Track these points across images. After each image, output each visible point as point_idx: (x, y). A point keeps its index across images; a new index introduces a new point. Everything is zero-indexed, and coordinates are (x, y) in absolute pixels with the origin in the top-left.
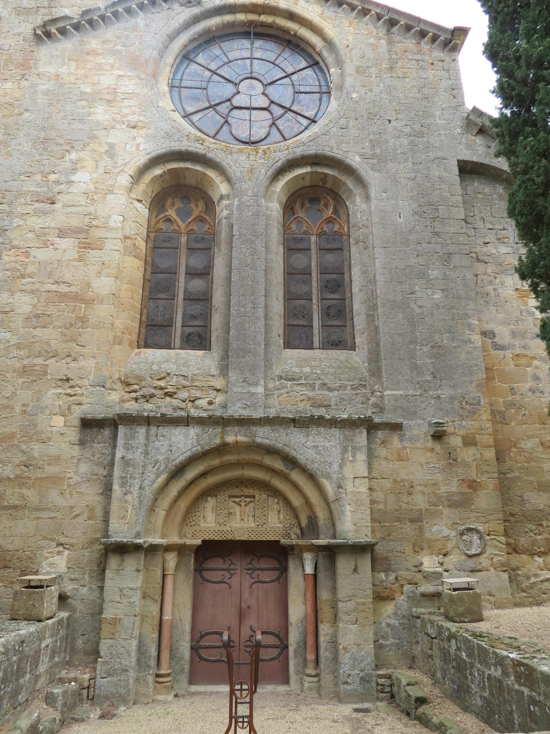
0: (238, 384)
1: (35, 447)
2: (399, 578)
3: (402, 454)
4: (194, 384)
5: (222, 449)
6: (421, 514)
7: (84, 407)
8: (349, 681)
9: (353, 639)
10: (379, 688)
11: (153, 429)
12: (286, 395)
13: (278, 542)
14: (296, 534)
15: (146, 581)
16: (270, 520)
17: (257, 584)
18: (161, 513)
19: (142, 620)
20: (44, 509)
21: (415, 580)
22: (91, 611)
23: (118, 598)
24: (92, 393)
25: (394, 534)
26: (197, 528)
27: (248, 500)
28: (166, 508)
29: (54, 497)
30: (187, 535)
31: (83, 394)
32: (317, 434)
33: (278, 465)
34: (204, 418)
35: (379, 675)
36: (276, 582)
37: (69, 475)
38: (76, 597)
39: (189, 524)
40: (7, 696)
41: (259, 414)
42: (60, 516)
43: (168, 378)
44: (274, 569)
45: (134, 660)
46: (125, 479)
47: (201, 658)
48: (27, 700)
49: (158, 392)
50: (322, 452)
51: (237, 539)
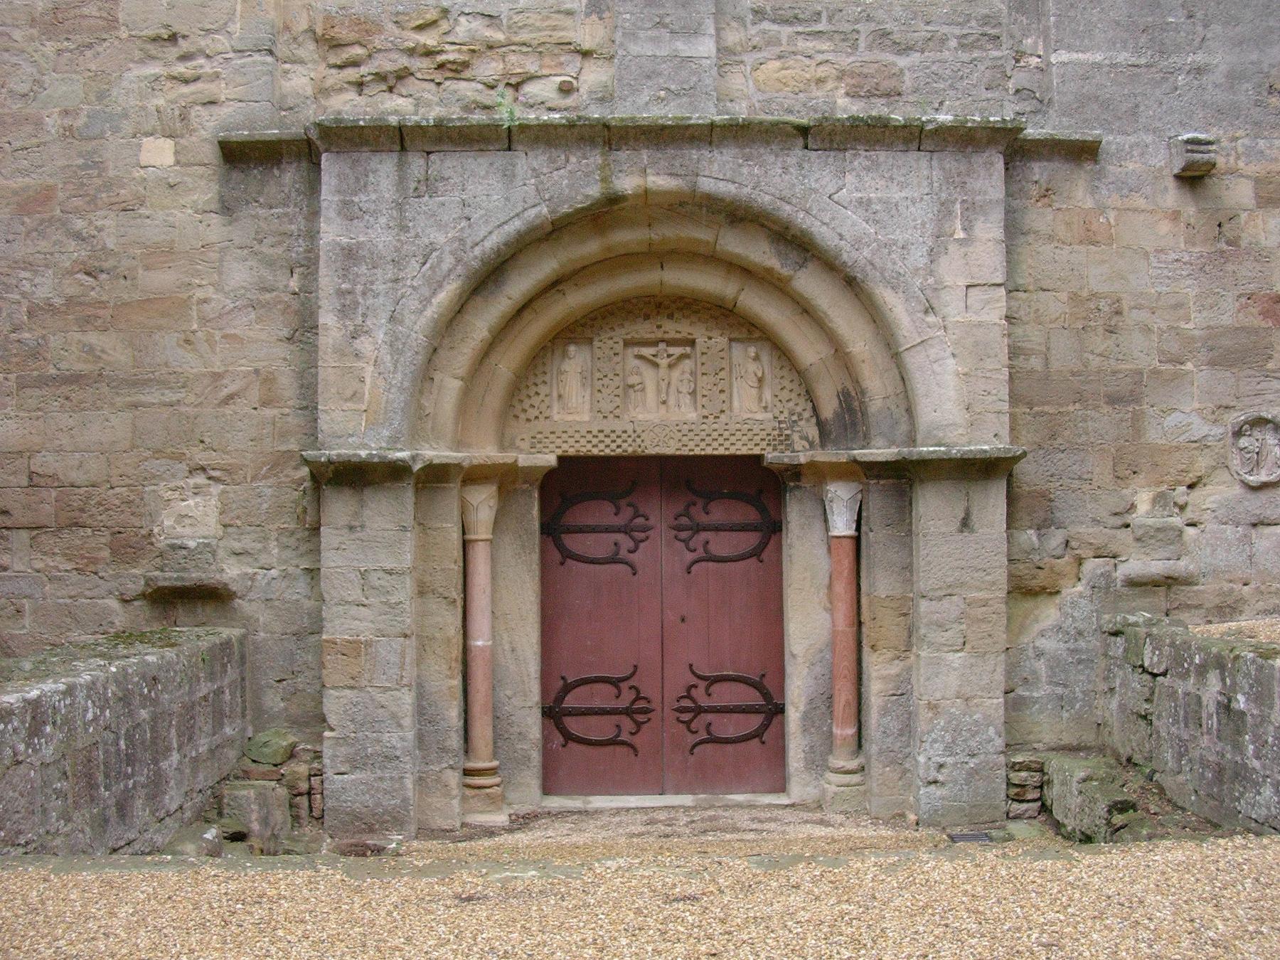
0: (642, 34)
1: (107, 222)
2: (1073, 544)
3: (1094, 228)
4: (517, 39)
5: (606, 211)
6: (1138, 383)
7: (224, 112)
8: (940, 778)
9: (950, 682)
10: (1013, 791)
11: (416, 164)
12: (778, 64)
13: (758, 458)
14: (806, 439)
15: (424, 551)
16: (736, 404)
17: (703, 564)
18: (450, 386)
19: (422, 649)
20: (146, 383)
21: (1114, 548)
22: (295, 628)
23: (356, 594)
24: (239, 71)
25: (1067, 433)
26: (541, 425)
27: (676, 351)
28: (462, 372)
29: (167, 349)
30: (518, 442)
31: (217, 76)
32: (868, 169)
33: (760, 253)
34: (556, 127)
35: (1015, 764)
36: (754, 560)
37: (200, 294)
38: (252, 595)
39: (523, 416)
40: (142, 792)
41: (706, 113)
42: (191, 398)
43: (444, 26)
44: (743, 528)
45: (410, 735)
46: (349, 297)
47: (568, 737)
48: (181, 808)
49: (419, 64)
50: (882, 216)
51: (652, 451)
